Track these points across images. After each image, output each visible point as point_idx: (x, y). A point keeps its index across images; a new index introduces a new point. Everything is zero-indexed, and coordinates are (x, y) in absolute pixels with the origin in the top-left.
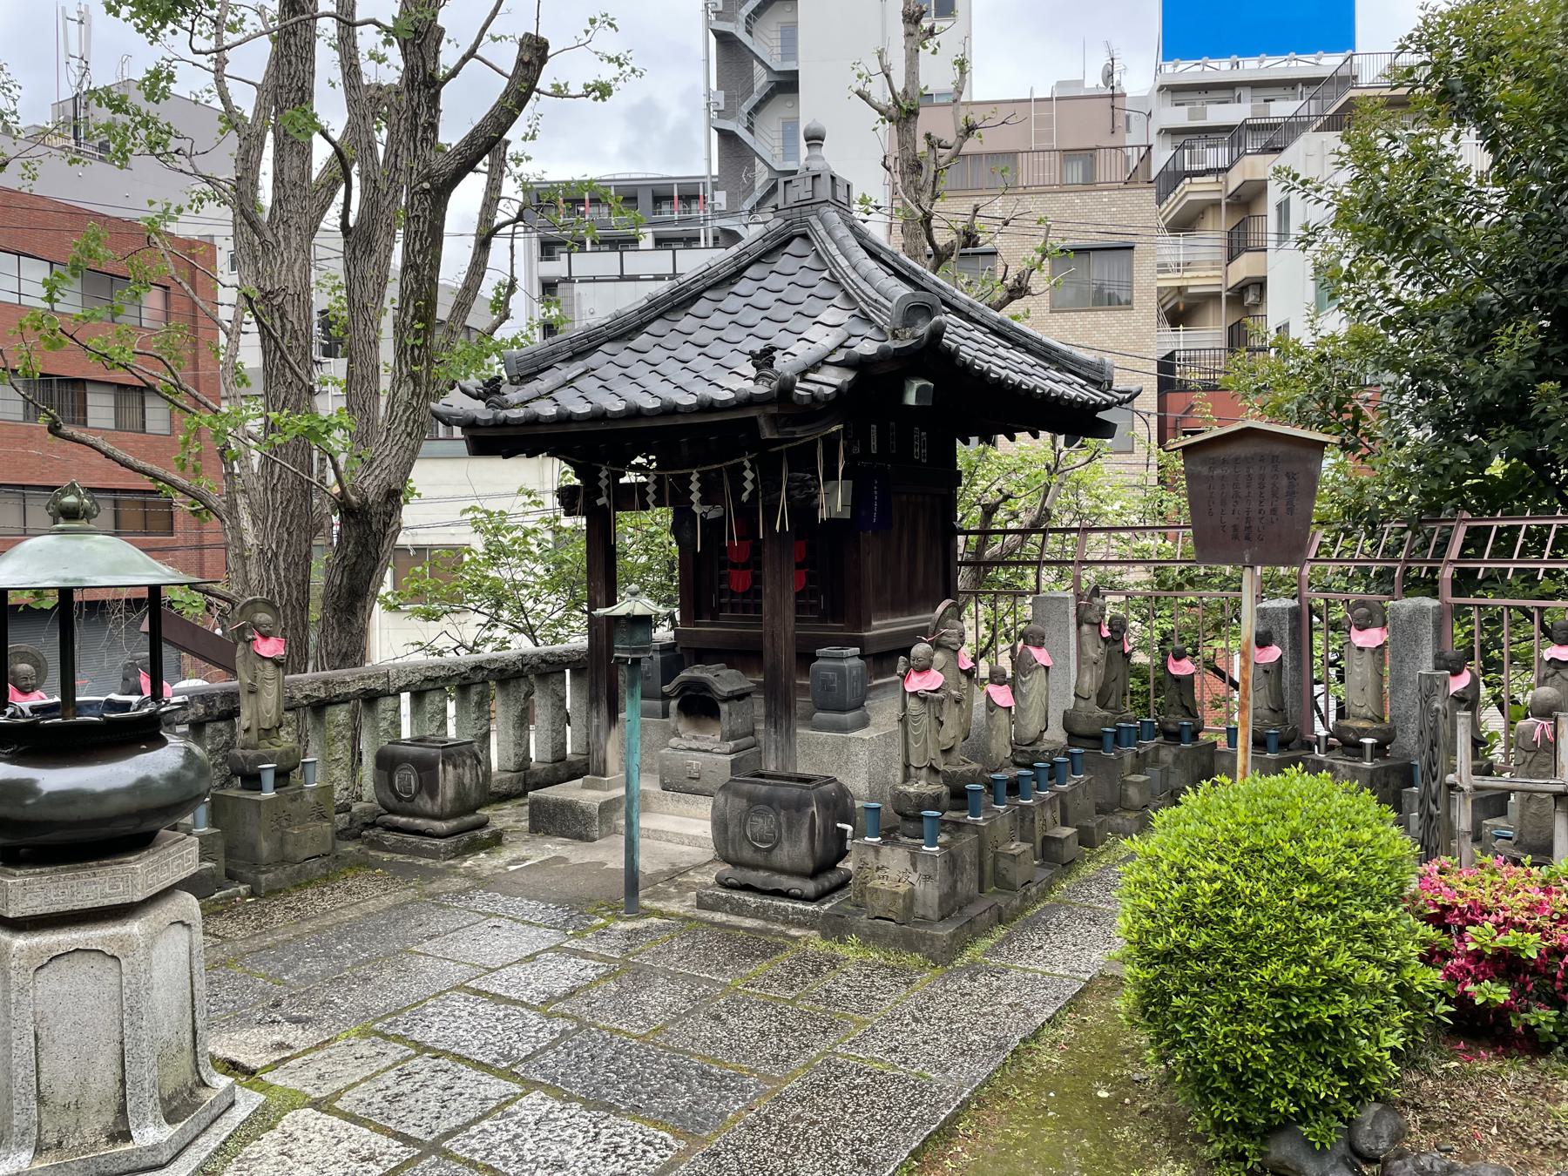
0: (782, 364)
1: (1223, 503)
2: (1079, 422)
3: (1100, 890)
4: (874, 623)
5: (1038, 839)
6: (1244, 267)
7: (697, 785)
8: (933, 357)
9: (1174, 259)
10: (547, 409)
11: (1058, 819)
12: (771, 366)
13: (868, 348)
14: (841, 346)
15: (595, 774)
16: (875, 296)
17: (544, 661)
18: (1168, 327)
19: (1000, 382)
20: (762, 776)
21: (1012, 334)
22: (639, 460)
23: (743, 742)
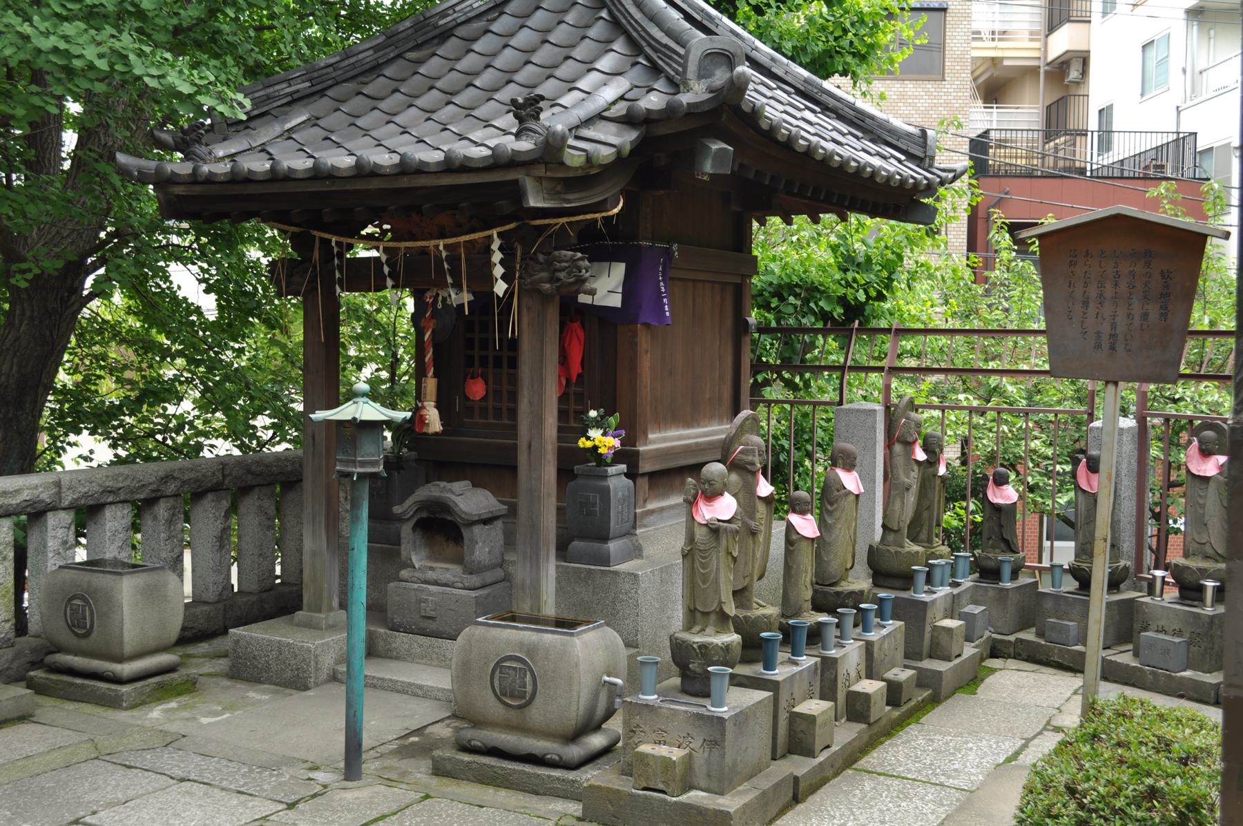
0: (554, 120)
1: (1086, 303)
2: (904, 202)
3: (908, 757)
4: (651, 436)
5: (841, 696)
6: (1063, 41)
7: (433, 626)
8: (729, 114)
9: (991, 27)
10: (260, 165)
11: (863, 674)
12: (537, 118)
13: (654, 101)
14: (622, 98)
15: (310, 610)
16: (665, 40)
17: (249, 471)
18: (980, 103)
19: (810, 151)
20: (513, 619)
21: (824, 98)
22: (370, 229)
23: (489, 576)
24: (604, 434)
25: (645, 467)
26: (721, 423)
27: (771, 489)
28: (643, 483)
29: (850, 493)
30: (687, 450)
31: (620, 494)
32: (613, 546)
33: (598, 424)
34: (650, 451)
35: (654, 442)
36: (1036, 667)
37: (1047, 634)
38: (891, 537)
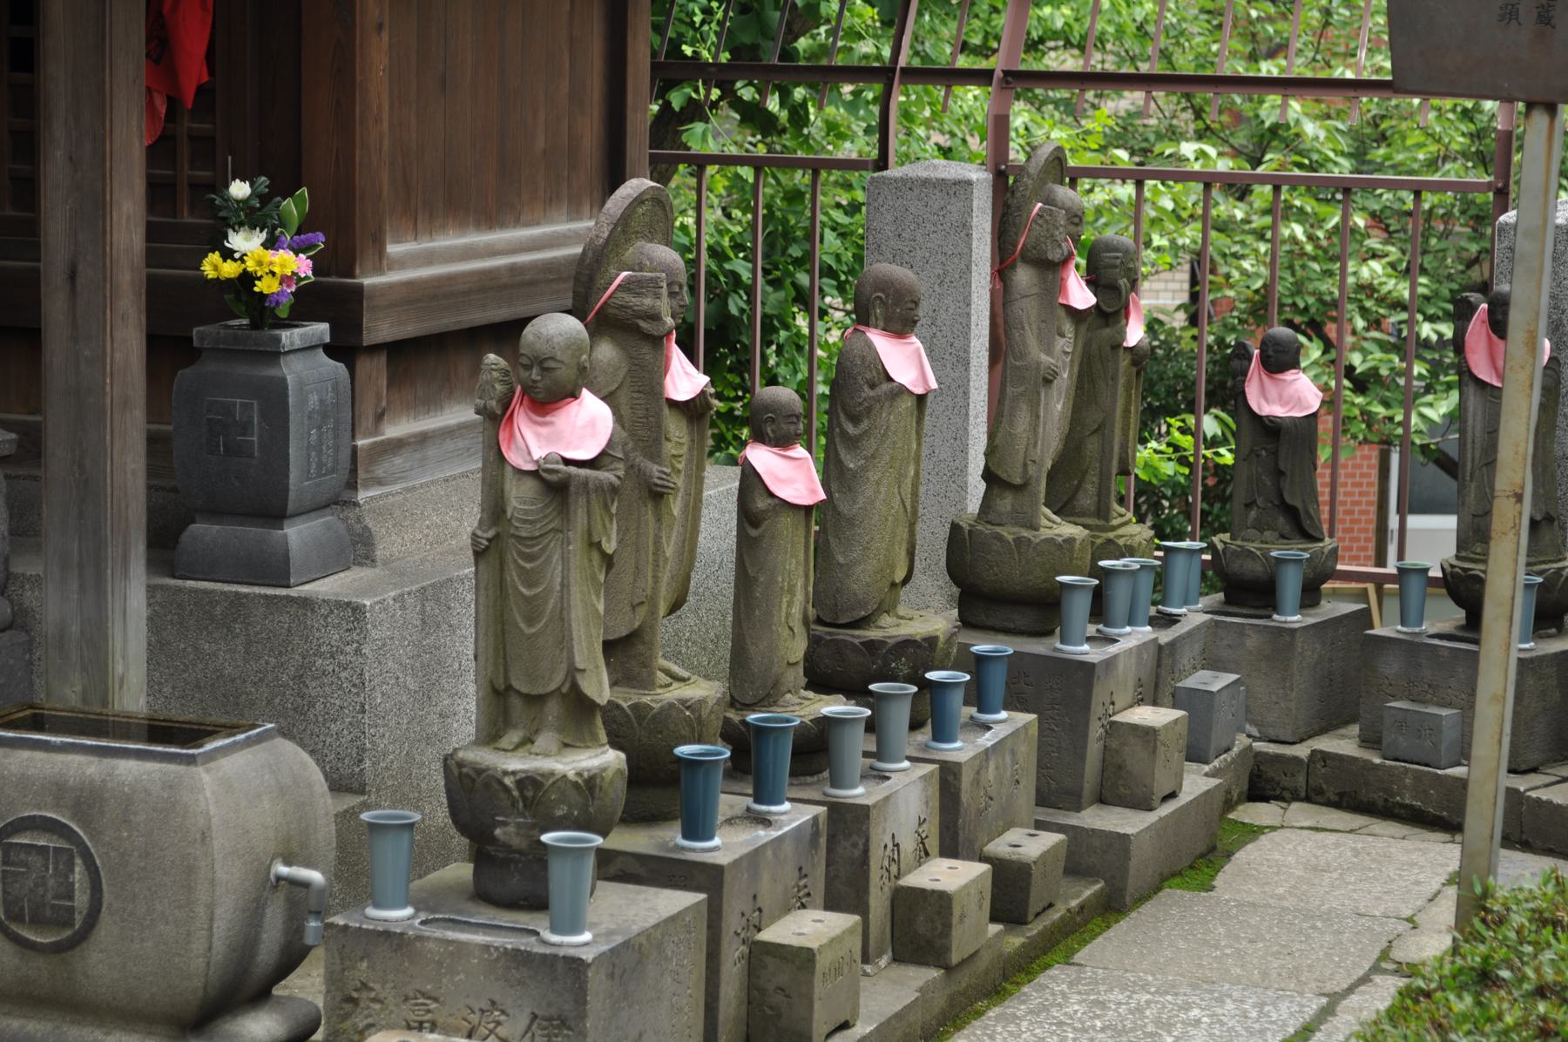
4: (393, 249)
25: (380, 328)
28: (374, 370)
29: (903, 390)
31: (313, 400)
32: (296, 534)
33: (251, 216)
35: (401, 263)
38: (1006, 503)
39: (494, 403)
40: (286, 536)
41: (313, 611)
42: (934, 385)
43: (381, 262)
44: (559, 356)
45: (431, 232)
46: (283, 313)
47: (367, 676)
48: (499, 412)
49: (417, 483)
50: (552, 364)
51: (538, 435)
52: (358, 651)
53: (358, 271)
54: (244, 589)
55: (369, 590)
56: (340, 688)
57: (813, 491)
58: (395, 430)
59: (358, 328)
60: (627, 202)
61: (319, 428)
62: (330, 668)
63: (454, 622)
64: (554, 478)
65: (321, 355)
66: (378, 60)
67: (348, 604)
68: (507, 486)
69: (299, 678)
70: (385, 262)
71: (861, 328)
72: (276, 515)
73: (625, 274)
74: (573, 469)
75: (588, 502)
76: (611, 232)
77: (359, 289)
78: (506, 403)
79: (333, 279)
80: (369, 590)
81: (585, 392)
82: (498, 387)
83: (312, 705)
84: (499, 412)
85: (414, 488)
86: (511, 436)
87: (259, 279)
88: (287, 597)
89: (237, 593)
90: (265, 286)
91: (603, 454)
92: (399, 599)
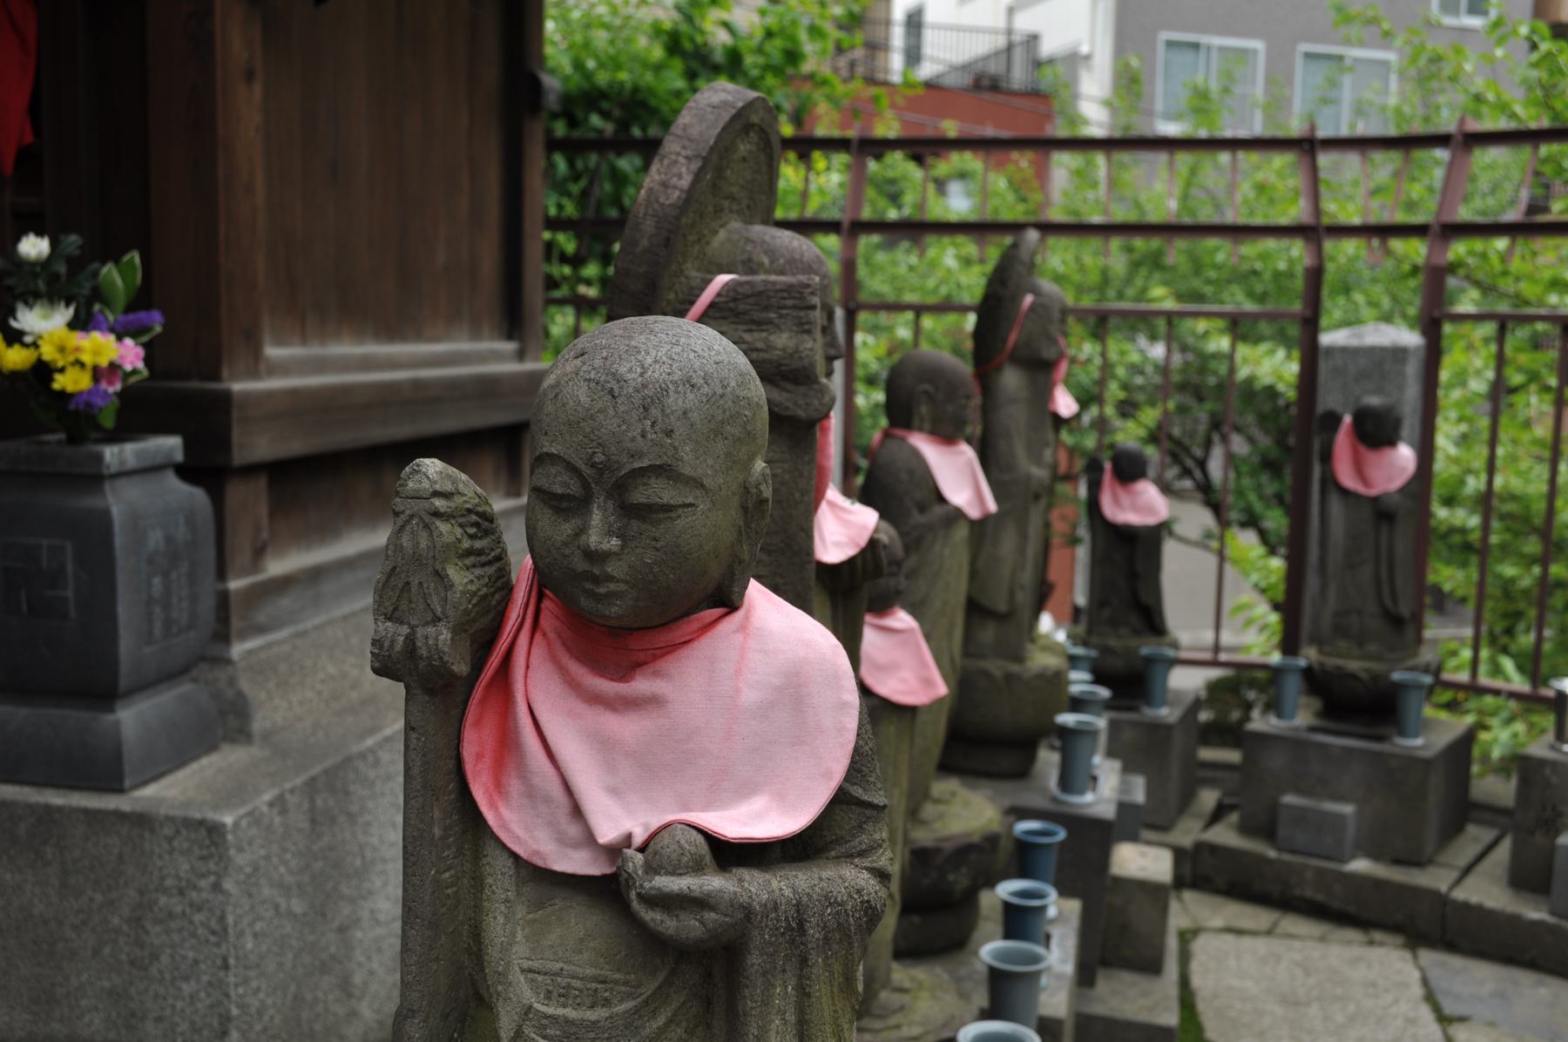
4: (272, 352)
24: (80, 323)
25: (256, 445)
26: (476, 335)
27: (867, 517)
28: (250, 499)
29: (958, 513)
30: (388, 399)
31: (155, 539)
32: (131, 719)
33: (46, 285)
34: (270, 395)
35: (275, 369)
36: (1259, 917)
37: (1283, 832)
38: (987, 633)
39: (443, 635)
40: (117, 723)
41: (152, 831)
42: (992, 506)
43: (256, 366)
44: (688, 460)
45: (323, 339)
46: (108, 421)
47: (230, 919)
48: (461, 668)
49: (309, 624)
50: (660, 492)
51: (606, 748)
52: (217, 887)
53: (225, 372)
54: (56, 798)
55: (234, 793)
56: (194, 935)
57: (928, 682)
58: (277, 567)
59: (224, 443)
60: (726, 116)
61: (166, 575)
62: (179, 909)
63: (354, 808)
64: (689, 926)
65: (172, 481)
66: (247, 114)
67: (202, 823)
68: (496, 927)
69: (136, 921)
70: (262, 367)
71: (899, 432)
72: (105, 694)
73: (723, 279)
74: (755, 885)
75: (803, 993)
76: (698, 177)
77: (226, 398)
78: (484, 632)
79: (195, 384)
80: (234, 793)
81: (757, 593)
82: (458, 576)
83: (155, 957)
84: (461, 668)
85: (304, 634)
86: (506, 745)
87: (62, 370)
88: (118, 815)
89: (48, 808)
90: (70, 381)
91: (840, 799)
92: (279, 803)
